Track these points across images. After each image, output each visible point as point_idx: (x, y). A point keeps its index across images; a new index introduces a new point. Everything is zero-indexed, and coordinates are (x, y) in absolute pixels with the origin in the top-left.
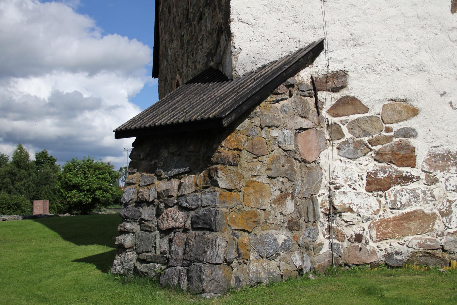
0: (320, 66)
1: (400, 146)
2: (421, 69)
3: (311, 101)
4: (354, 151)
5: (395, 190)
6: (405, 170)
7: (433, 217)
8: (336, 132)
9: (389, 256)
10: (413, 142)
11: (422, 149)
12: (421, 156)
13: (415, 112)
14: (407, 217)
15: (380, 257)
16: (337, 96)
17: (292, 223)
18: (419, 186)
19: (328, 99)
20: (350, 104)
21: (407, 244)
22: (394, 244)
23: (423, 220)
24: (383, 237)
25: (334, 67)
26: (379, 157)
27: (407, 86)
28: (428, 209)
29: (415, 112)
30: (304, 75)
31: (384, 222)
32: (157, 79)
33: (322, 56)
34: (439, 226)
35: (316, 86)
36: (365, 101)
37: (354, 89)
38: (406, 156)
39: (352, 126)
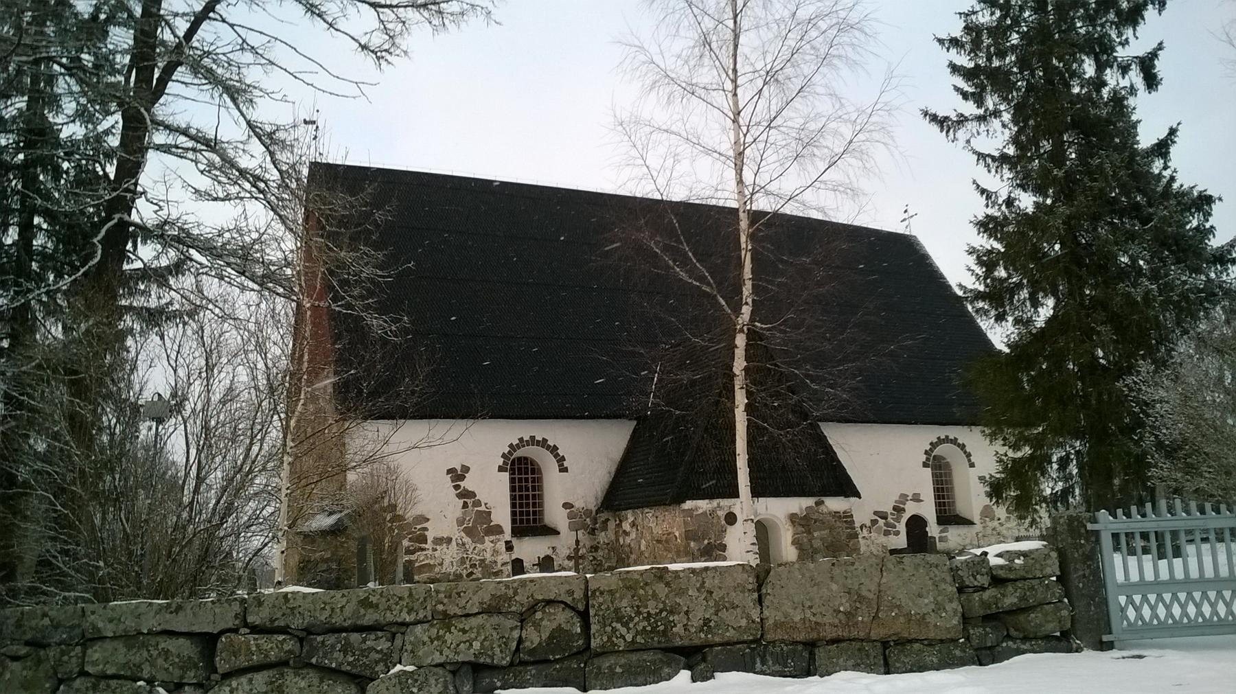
11: (430, 536)
18: (430, 552)
34: (437, 570)
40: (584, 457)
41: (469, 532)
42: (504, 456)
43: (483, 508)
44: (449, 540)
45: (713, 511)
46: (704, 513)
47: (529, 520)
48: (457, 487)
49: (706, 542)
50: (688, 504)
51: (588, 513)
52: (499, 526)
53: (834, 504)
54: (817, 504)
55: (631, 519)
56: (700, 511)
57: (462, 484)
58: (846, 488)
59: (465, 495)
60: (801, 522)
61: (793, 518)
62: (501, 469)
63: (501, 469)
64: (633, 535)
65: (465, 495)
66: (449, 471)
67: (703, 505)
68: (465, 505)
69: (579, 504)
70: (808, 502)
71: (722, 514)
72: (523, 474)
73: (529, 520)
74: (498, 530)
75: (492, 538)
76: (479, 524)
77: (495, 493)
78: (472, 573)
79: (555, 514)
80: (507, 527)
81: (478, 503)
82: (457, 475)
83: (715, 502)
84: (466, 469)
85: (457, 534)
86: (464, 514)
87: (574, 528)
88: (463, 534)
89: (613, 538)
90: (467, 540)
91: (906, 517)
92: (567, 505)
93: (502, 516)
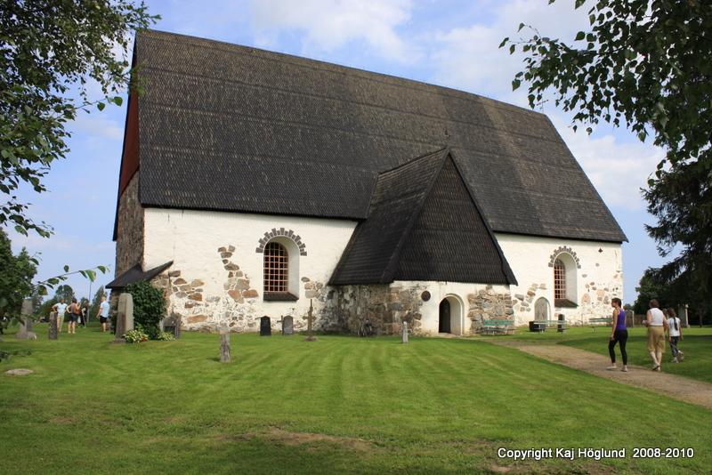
0: (172, 269)
1: (197, 294)
2: (206, 270)
3: (168, 280)
4: (182, 295)
5: (56, 287)
6: (199, 302)
7: (206, 317)
8: (176, 289)
9: (191, 328)
10: (201, 293)
11: (204, 295)
12: (204, 298)
13: (202, 284)
14: (197, 317)
15: (188, 329)
16: (176, 278)
17: (230, 388)
18: (203, 307)
19: (173, 279)
20: (181, 281)
21: (197, 325)
22: (192, 325)
23: (203, 318)
24: (189, 322)
25: (176, 269)
26: (190, 297)
27: (200, 276)
28: (205, 314)
29: (202, 284)
30: (166, 272)
31: (190, 318)
32: (115, 242)
33: (173, 266)
34: (208, 320)
35: (170, 275)
36: (185, 279)
37: (182, 276)
38: (198, 297)
39: (181, 288)
40: (322, 246)
41: (233, 294)
42: (261, 241)
43: (243, 278)
44: (218, 300)
45: (414, 289)
46: (407, 291)
47: (277, 288)
48: (225, 261)
49: (407, 312)
50: (396, 284)
51: (319, 286)
52: (255, 291)
53: (499, 289)
54: (487, 289)
55: (350, 292)
56: (405, 289)
57: (229, 259)
58: (507, 278)
59: (230, 267)
60: (478, 301)
61: (470, 297)
62: (258, 251)
63: (258, 251)
64: (351, 303)
65: (230, 267)
66: (220, 250)
67: (406, 285)
68: (231, 275)
69: (313, 279)
70: (482, 287)
71: (420, 292)
72: (276, 252)
73: (277, 288)
74: (254, 294)
75: (249, 299)
76: (241, 291)
77: (254, 267)
78: (233, 324)
79: (296, 285)
80: (261, 292)
81: (240, 274)
82: (226, 253)
83: (415, 283)
84: (232, 249)
85: (224, 295)
86: (230, 281)
87: (308, 296)
88: (228, 295)
89: (336, 304)
90: (231, 300)
91: (535, 299)
92: (305, 279)
93: (258, 284)
